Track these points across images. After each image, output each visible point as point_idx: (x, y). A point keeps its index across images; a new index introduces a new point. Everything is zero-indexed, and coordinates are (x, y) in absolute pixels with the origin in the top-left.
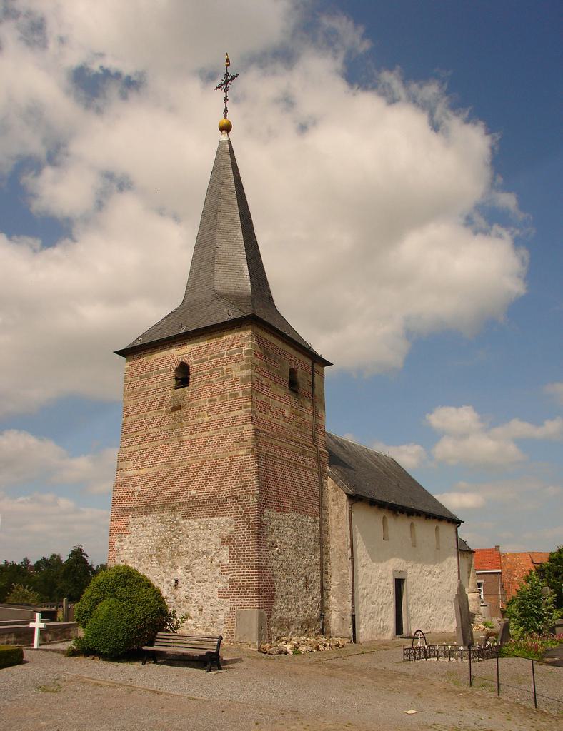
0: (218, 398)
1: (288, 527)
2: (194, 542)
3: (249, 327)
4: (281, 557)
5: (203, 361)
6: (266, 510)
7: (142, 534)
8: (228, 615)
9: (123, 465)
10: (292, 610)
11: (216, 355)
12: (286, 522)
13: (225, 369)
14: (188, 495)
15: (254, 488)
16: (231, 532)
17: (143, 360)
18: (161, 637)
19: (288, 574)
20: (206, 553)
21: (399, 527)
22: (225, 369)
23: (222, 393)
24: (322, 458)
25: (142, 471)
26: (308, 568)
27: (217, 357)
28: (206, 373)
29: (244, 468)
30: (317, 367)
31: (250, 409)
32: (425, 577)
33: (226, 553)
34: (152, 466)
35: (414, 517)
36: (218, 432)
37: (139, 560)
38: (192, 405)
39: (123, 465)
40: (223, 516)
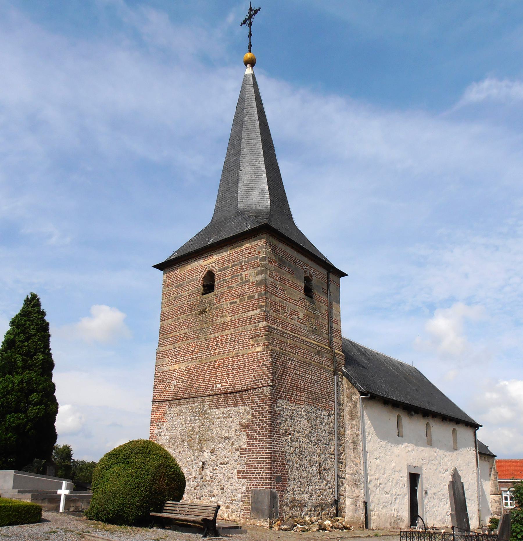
0: (238, 300)
1: (299, 416)
2: (218, 429)
3: (263, 236)
4: (294, 443)
5: (225, 269)
6: (280, 401)
7: (176, 422)
8: (245, 493)
9: (161, 362)
10: (305, 493)
11: (236, 263)
12: (300, 413)
13: (243, 276)
14: (214, 388)
15: (268, 381)
16: (248, 420)
17: (178, 272)
18: (169, 505)
19: (302, 460)
20: (228, 438)
21: (414, 426)
22: (243, 276)
23: (241, 296)
24: (338, 360)
25: (176, 366)
26: (323, 456)
27: (237, 265)
28: (228, 280)
29: (260, 363)
30: (331, 276)
31: (264, 309)
32: (441, 475)
33: (244, 438)
34: (183, 362)
35: (430, 418)
36: (237, 330)
37: (173, 445)
38: (216, 308)
39: (161, 362)
40: (242, 406)
